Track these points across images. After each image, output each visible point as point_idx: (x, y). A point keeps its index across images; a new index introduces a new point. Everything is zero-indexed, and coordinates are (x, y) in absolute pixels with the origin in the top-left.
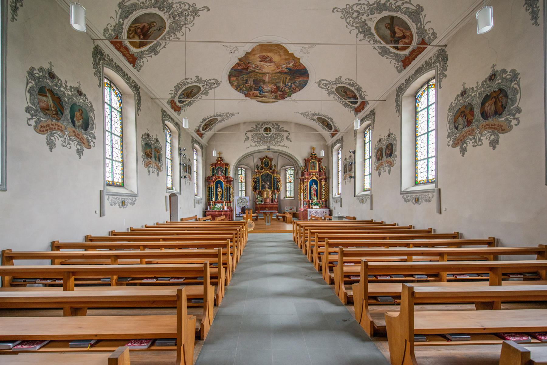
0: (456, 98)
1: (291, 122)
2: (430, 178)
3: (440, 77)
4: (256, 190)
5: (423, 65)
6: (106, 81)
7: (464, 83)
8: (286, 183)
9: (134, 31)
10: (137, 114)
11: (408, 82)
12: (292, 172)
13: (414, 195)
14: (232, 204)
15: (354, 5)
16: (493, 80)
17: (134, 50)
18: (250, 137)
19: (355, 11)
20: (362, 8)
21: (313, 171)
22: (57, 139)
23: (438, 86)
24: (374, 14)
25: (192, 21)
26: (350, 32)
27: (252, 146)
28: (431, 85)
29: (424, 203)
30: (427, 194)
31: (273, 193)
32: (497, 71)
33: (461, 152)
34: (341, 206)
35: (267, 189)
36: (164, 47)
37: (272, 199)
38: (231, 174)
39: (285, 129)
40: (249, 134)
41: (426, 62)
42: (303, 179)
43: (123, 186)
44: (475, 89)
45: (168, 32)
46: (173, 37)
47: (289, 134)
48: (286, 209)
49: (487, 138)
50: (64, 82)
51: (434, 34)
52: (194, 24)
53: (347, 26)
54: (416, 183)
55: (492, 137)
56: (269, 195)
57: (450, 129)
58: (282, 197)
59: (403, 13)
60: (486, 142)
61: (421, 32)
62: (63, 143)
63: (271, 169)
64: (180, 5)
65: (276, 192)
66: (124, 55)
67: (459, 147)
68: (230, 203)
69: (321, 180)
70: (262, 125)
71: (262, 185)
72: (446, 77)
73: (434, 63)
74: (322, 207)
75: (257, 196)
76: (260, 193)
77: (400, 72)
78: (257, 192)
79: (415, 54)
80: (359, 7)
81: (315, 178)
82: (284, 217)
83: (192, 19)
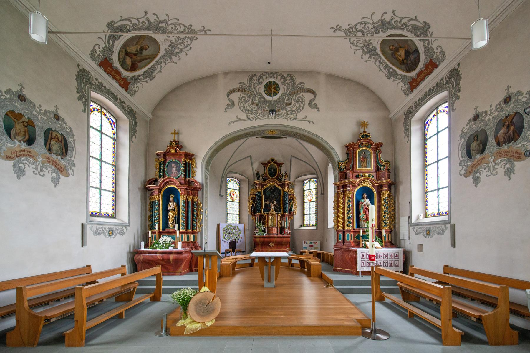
0: (468, 123)
1: (319, 73)
2: (441, 210)
3: (453, 99)
4: (255, 213)
5: (434, 87)
6: (95, 106)
7: (508, 87)
8: (303, 203)
9: (125, 53)
10: (131, 140)
11: (418, 105)
12: (313, 185)
13: (425, 227)
14: (198, 236)
15: (358, 23)
16: (508, 103)
17: (125, 74)
18: (237, 102)
19: (360, 31)
20: (366, 27)
21: (364, 170)
22: (27, 166)
23: (451, 111)
24: (379, 32)
25: (189, 45)
26: (355, 53)
27: (240, 120)
28: (440, 111)
29: (436, 236)
30: (439, 226)
31: (282, 218)
32: (512, 94)
33: (473, 182)
34: (453, 244)
35: (272, 211)
36: (160, 72)
37: (281, 228)
38: (198, 176)
39: (306, 86)
40: (235, 97)
41: (437, 83)
42: (344, 186)
43: (114, 218)
44: (489, 113)
45: (164, 56)
46: (169, 61)
47: (315, 96)
48: (304, 245)
49: (501, 167)
50: (37, 105)
51: (442, 53)
52: (191, 48)
53: (350, 46)
54: (425, 216)
55: (507, 166)
56: (275, 222)
57: (462, 157)
58: (297, 225)
59: (409, 31)
60: (501, 171)
61: (429, 50)
62: (34, 170)
63: (280, 180)
64: (176, 27)
65: (287, 217)
66: (114, 78)
67: (471, 177)
68: (193, 233)
69: (380, 188)
70: (261, 77)
71: (266, 205)
72: (459, 98)
73: (445, 84)
74: (386, 247)
75: (257, 223)
76: (262, 218)
77: (407, 95)
78: (257, 217)
79: (422, 75)
80: (363, 26)
81: (368, 184)
82: (302, 262)
83: (189, 42)
